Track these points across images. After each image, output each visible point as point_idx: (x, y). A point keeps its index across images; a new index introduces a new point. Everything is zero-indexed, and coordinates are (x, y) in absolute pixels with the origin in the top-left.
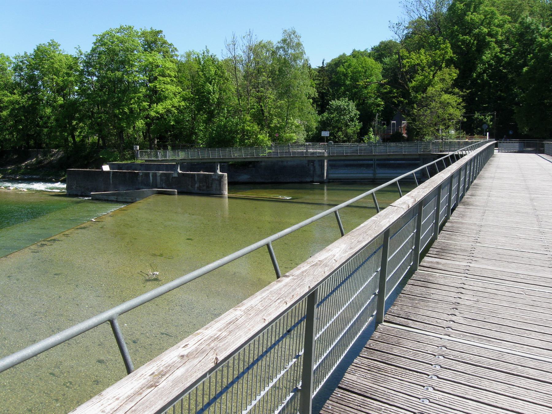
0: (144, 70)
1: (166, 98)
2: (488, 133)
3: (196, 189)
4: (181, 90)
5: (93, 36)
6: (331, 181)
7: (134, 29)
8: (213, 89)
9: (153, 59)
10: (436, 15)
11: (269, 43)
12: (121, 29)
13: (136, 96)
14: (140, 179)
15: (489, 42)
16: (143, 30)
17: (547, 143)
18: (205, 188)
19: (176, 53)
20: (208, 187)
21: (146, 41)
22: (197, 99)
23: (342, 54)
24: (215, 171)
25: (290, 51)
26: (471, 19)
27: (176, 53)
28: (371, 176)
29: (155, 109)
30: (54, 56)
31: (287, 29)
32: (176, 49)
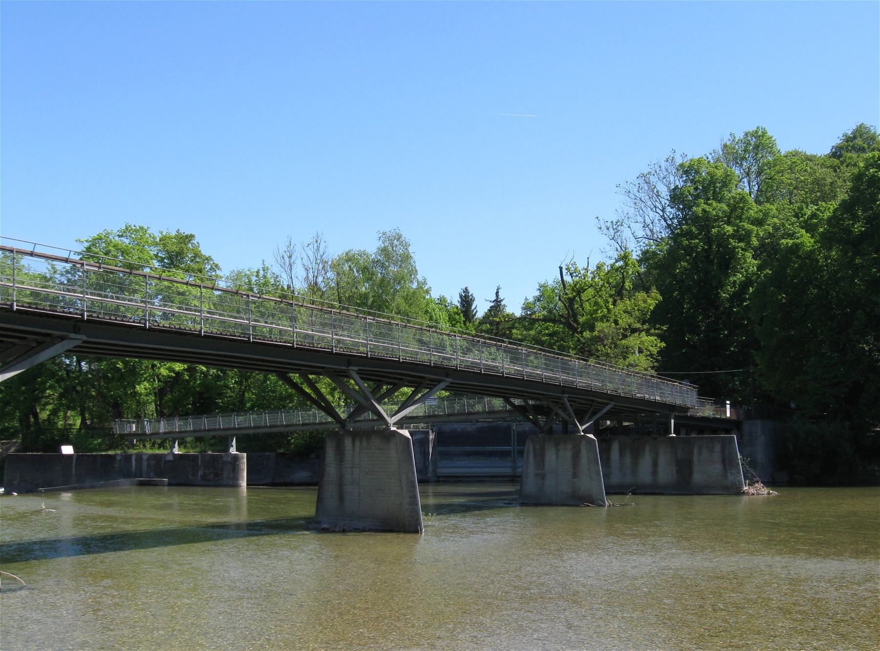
3: (199, 478)
5: (77, 241)
6: (442, 479)
7: (149, 232)
10: (131, 268)
11: (362, 254)
12: (126, 231)
14: (117, 465)
15: (735, 248)
17: (31, 286)
18: (212, 476)
19: (218, 272)
20: (216, 475)
24: (227, 449)
25: (393, 269)
26: (704, 211)
27: (218, 272)
28: (508, 471)
31: (387, 230)
32: (216, 266)
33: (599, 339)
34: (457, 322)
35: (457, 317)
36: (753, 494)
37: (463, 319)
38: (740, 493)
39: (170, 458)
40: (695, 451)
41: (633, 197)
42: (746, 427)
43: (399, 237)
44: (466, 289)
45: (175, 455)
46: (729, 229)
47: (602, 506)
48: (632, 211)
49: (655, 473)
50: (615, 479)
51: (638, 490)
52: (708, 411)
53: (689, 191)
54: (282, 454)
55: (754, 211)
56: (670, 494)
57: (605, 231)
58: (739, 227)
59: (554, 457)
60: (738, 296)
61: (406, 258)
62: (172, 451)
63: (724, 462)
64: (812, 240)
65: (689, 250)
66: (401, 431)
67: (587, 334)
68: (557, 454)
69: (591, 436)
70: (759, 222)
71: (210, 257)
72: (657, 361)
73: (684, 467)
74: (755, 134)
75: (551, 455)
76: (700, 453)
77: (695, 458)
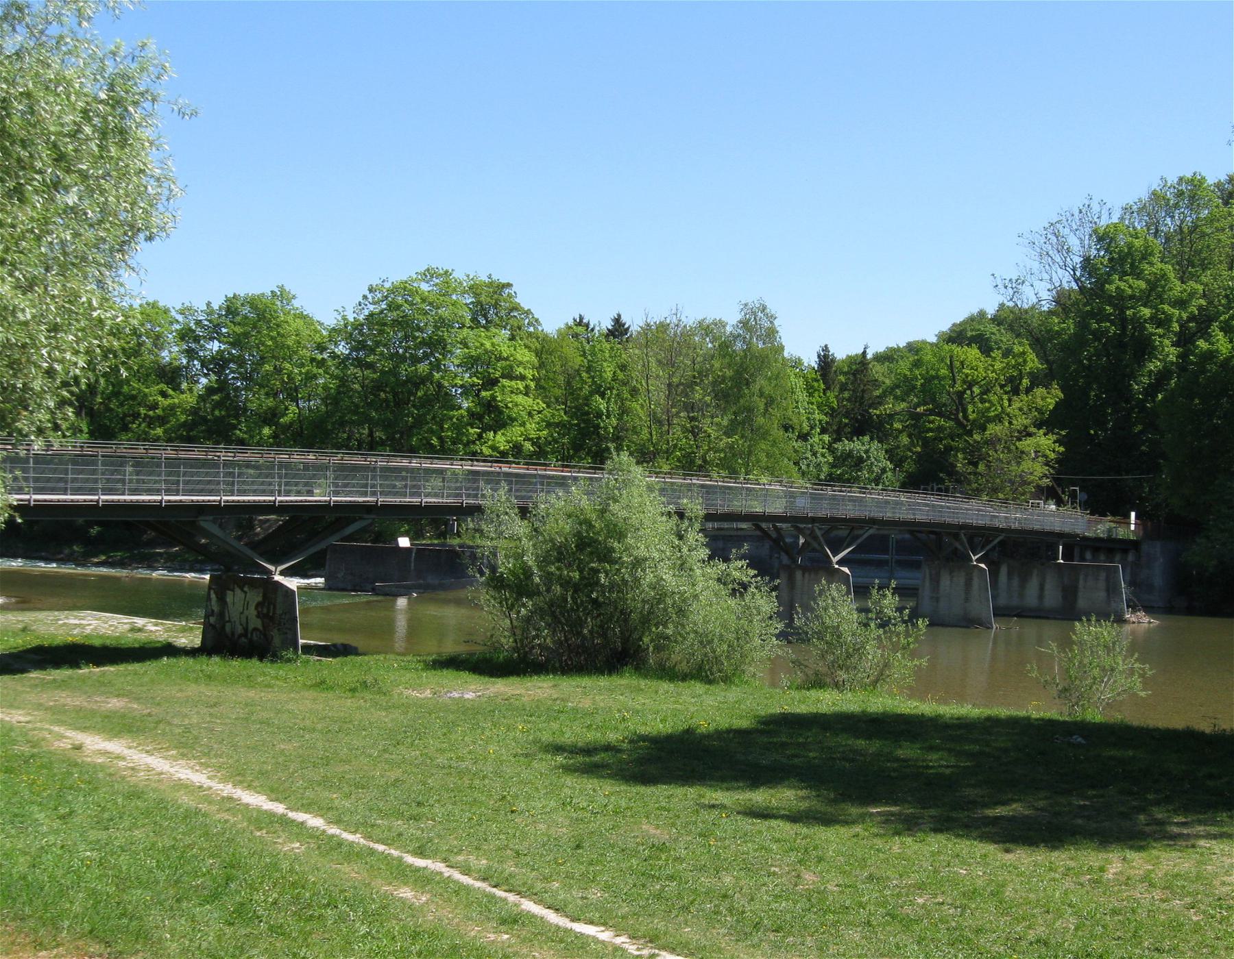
0: (470, 363)
1: (513, 420)
2: (1133, 514)
4: (544, 405)
8: (608, 408)
9: (493, 345)
11: (721, 324)
12: (429, 274)
13: (454, 416)
16: (471, 277)
21: (479, 303)
22: (576, 425)
23: (975, 311)
26: (1117, 288)
29: (490, 443)
30: (287, 322)
31: (750, 301)
32: (537, 320)
33: (992, 442)
34: (816, 390)
35: (816, 384)
36: (1134, 623)
37: (823, 386)
38: (1120, 620)
40: (1081, 577)
41: (1039, 250)
42: (1145, 547)
43: (764, 309)
44: (826, 346)
46: (1146, 312)
48: (1036, 266)
49: (1041, 597)
50: (1002, 601)
51: (1022, 613)
52: (1102, 527)
53: (1102, 263)
55: (1177, 288)
56: (1055, 619)
57: (1003, 290)
58: (1158, 310)
59: (948, 583)
60: (1151, 391)
61: (772, 333)
63: (1108, 590)
64: (1230, 346)
65: (1098, 335)
66: (842, 568)
67: (977, 437)
68: (951, 580)
69: (983, 566)
70: (1181, 303)
71: (529, 310)
72: (1053, 468)
73: (1070, 593)
74: (1191, 181)
75: (945, 581)
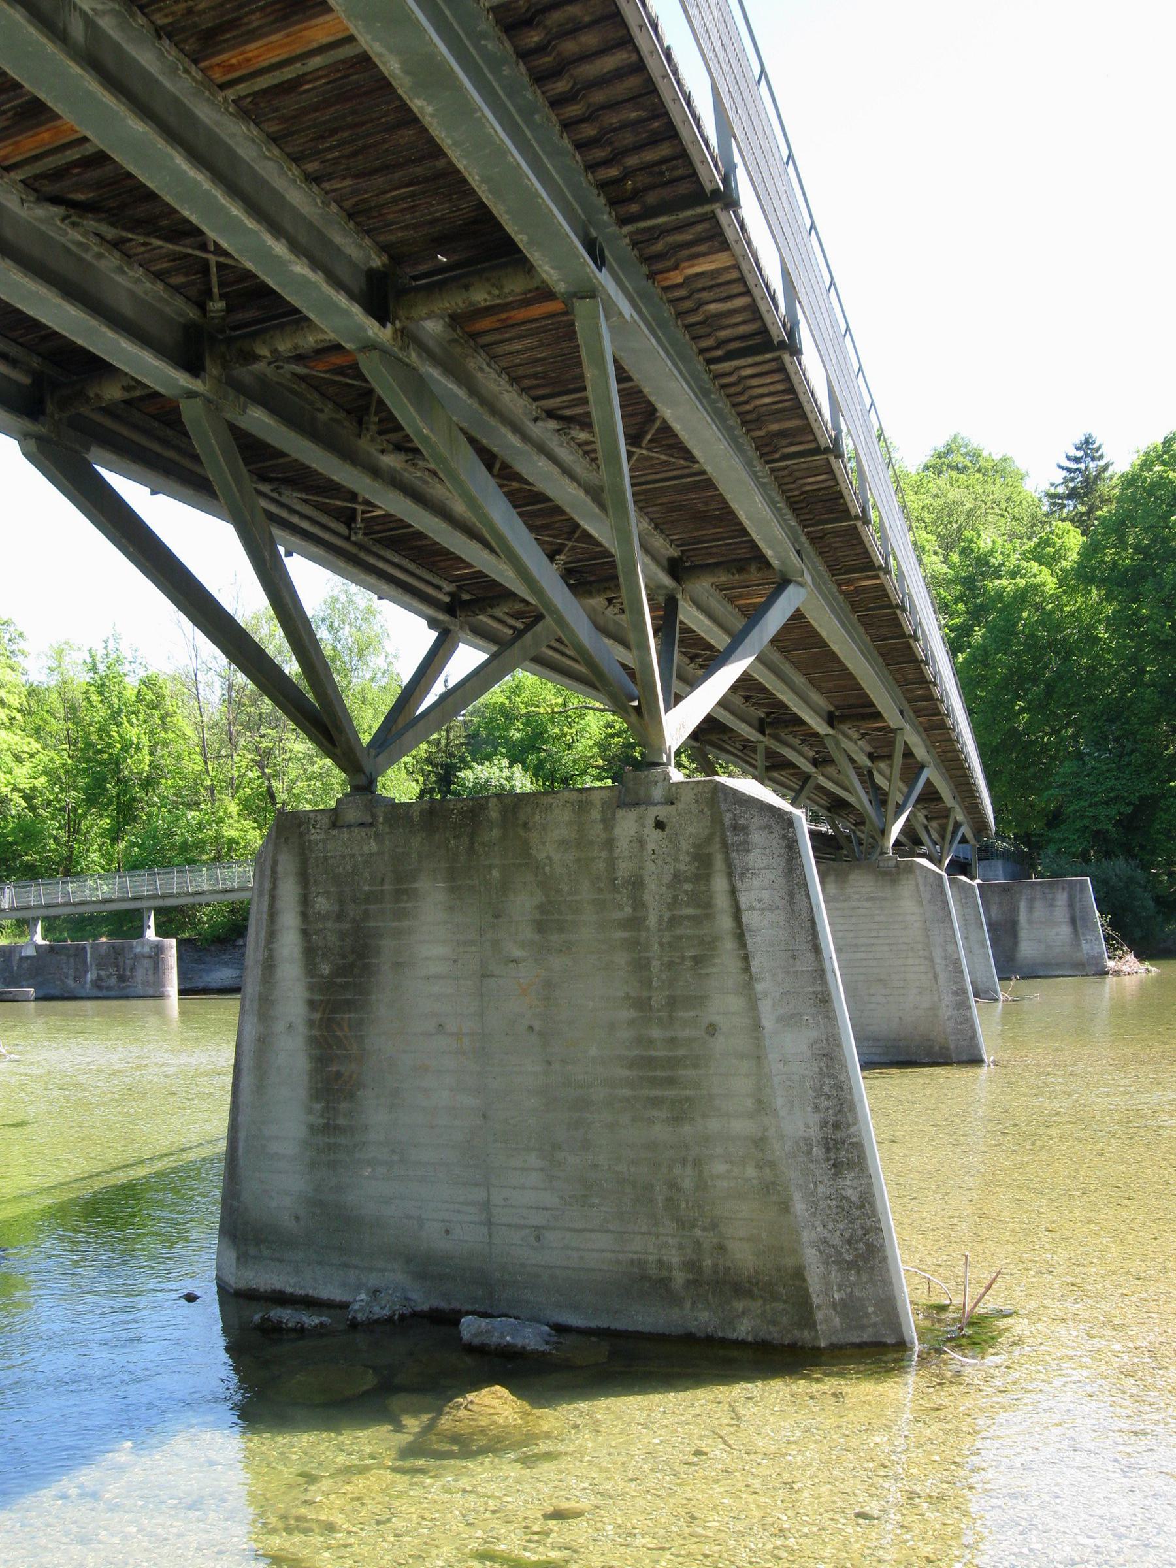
3: (88, 985)
18: (113, 981)
20: (122, 978)
24: (139, 933)
39: (30, 952)
40: (1023, 905)
45: (38, 947)
47: (996, 1000)
54: (188, 941)
62: (32, 939)
63: (1073, 921)
76: (1031, 909)
77: (1023, 917)
